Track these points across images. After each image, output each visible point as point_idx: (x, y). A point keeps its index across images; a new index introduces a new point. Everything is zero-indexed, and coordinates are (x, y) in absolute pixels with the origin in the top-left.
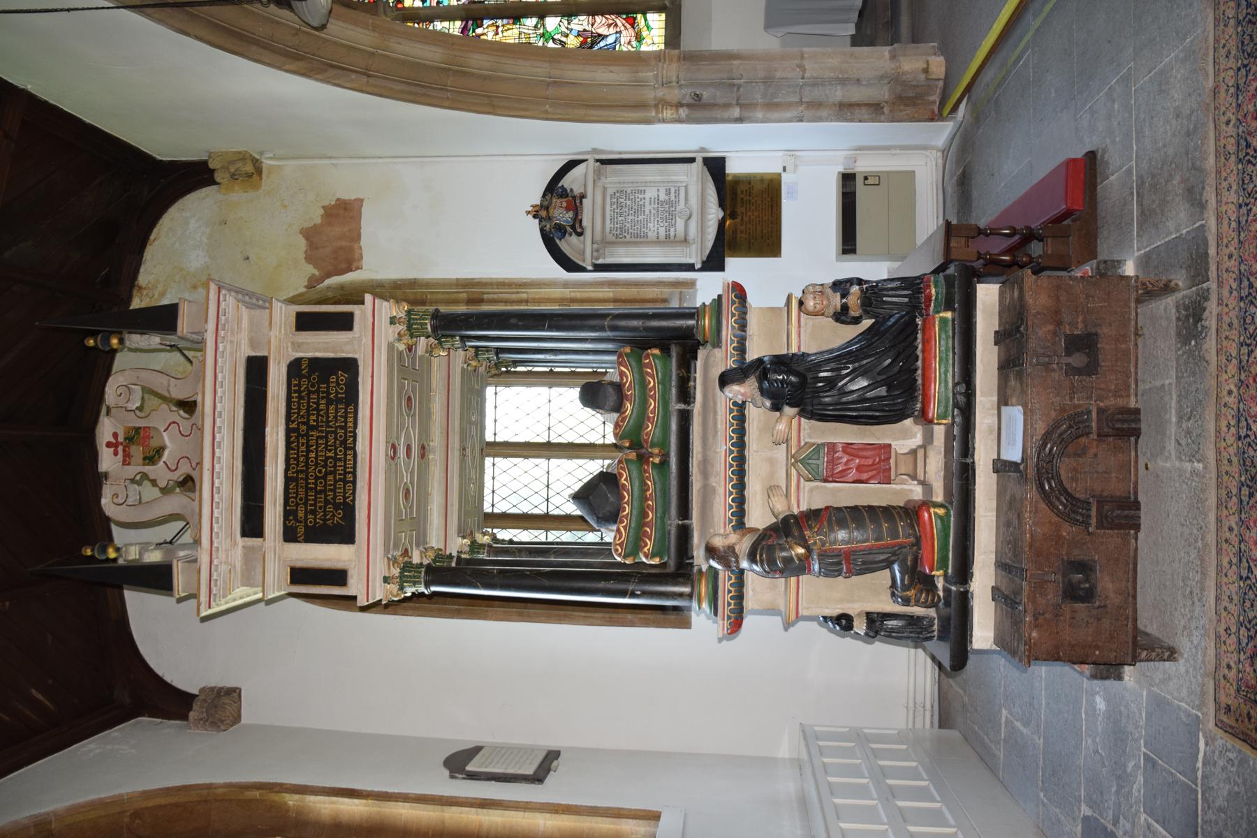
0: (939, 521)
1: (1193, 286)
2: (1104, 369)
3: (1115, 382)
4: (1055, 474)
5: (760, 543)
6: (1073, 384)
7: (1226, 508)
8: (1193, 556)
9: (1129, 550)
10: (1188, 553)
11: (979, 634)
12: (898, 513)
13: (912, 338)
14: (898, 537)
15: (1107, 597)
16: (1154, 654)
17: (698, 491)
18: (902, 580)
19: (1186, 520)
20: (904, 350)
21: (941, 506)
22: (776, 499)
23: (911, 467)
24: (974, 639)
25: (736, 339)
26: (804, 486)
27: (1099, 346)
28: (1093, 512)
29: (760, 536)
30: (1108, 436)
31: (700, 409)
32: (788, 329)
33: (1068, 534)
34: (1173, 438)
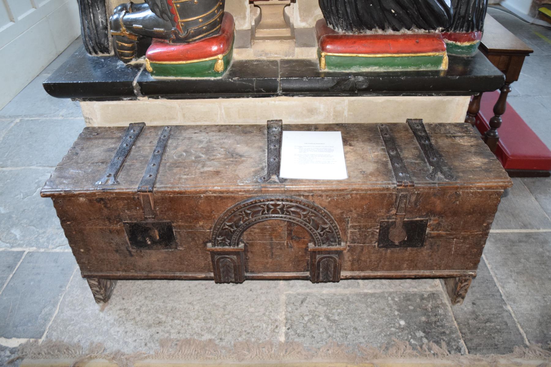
0: (208, 64)
2: (384, 252)
4: (267, 215)
11: (95, 106)
12: (213, 14)
18: (136, 21)
20: (408, 14)
21: (227, 62)
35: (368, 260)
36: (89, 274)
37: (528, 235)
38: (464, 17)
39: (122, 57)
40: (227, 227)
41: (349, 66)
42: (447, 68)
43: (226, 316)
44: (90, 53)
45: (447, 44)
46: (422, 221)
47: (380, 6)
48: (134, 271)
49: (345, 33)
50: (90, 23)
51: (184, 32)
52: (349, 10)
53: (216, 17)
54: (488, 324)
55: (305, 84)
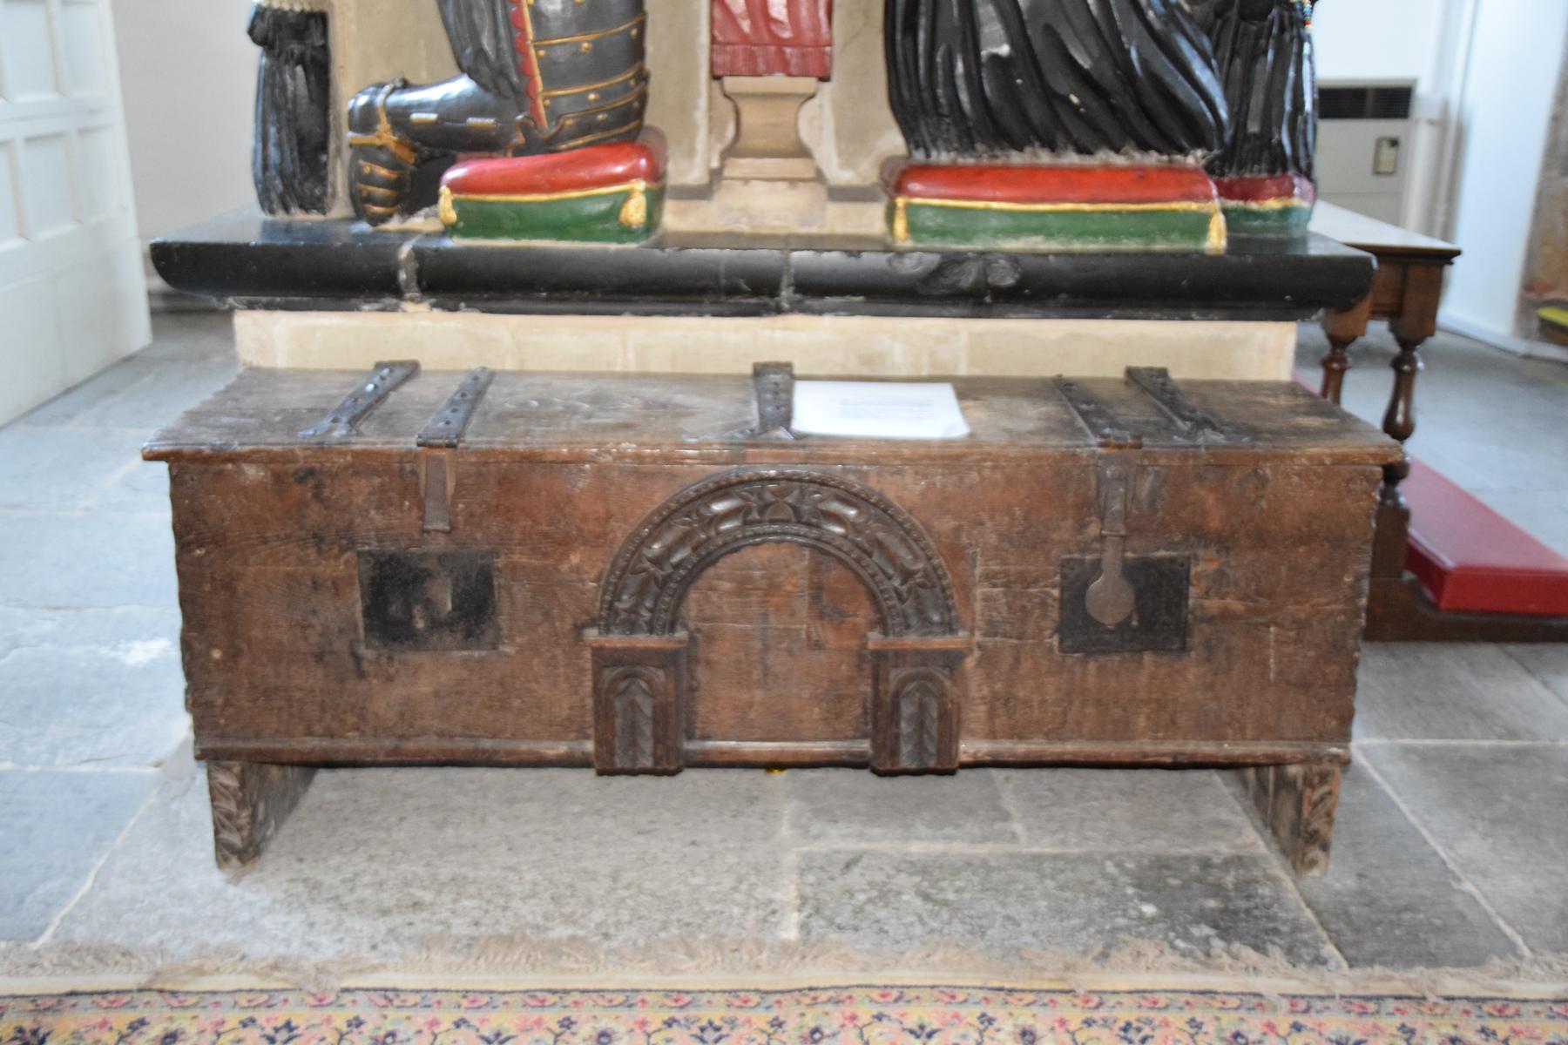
0: (603, 206)
1: (1318, 914)
2: (1078, 670)
3: (1036, 699)
4: (757, 528)
6: (1036, 582)
7: (670, 1023)
8: (524, 910)
9: (536, 737)
10: (533, 895)
13: (1147, 133)
14: (551, 80)
15: (390, 679)
16: (231, 807)
18: (421, 106)
19: (628, 887)
23: (760, 143)
24: (260, 316)
27: (1148, 658)
28: (642, 640)
30: (877, 678)
33: (577, 570)
34: (864, 846)
35: (1036, 699)
36: (219, 744)
37: (1519, 753)
40: (647, 564)
41: (966, 235)
43: (620, 892)
46: (1172, 560)
48: (356, 734)
54: (1407, 916)
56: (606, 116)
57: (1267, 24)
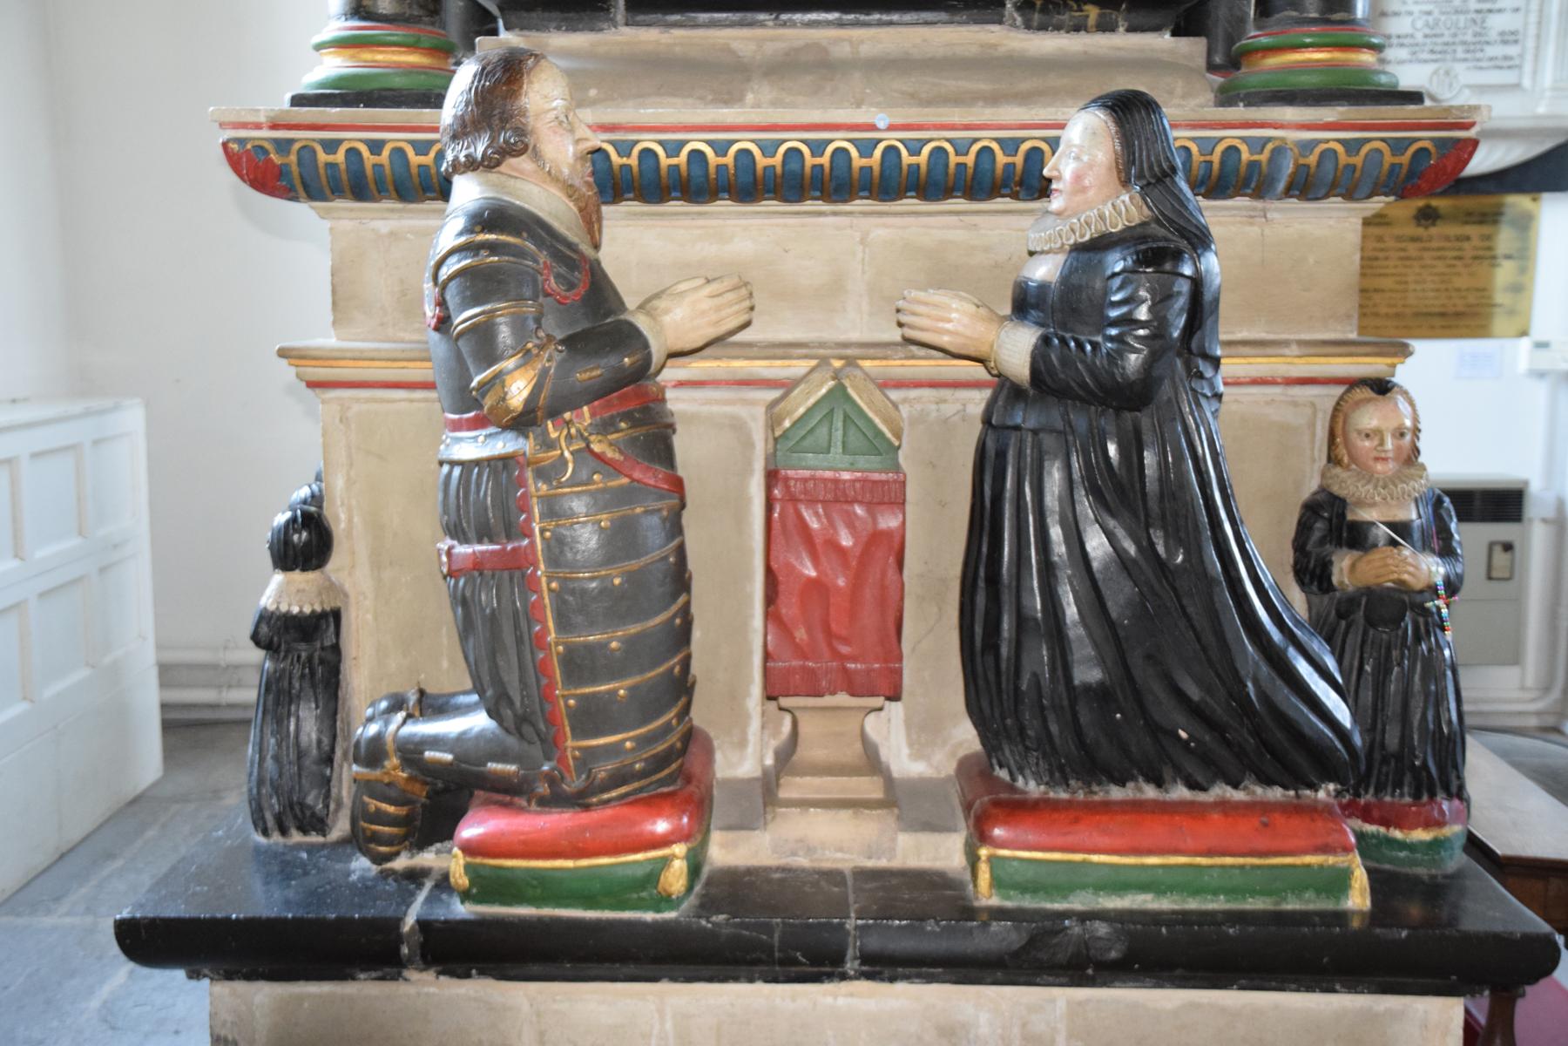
0: (640, 872)
5: (540, 243)
12: (667, 729)
17: (727, 50)
18: (436, 742)
20: (1228, 744)
21: (694, 870)
22: (707, 304)
25: (1263, 157)
26: (752, 403)
29: (571, 246)
31: (1002, 51)
32: (1286, 343)
38: (1399, 757)
39: (372, 846)
41: (1065, 891)
42: (1368, 903)
44: (265, 833)
45: (1360, 836)
47: (1145, 719)
49: (1046, 793)
50: (284, 743)
51: (579, 776)
52: (1054, 728)
53: (673, 739)
55: (934, 937)
56: (643, 764)
57: (1400, 632)
